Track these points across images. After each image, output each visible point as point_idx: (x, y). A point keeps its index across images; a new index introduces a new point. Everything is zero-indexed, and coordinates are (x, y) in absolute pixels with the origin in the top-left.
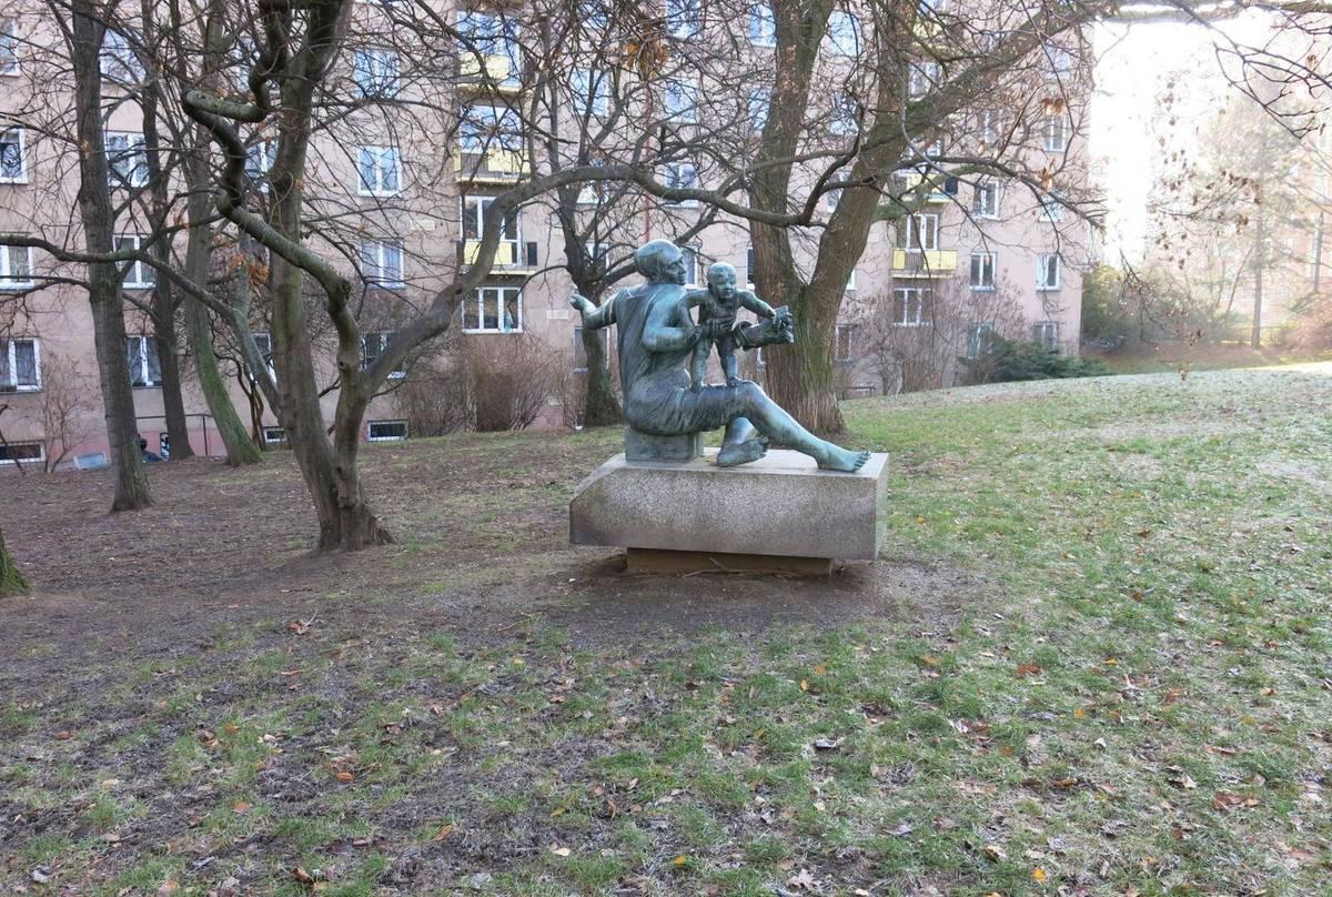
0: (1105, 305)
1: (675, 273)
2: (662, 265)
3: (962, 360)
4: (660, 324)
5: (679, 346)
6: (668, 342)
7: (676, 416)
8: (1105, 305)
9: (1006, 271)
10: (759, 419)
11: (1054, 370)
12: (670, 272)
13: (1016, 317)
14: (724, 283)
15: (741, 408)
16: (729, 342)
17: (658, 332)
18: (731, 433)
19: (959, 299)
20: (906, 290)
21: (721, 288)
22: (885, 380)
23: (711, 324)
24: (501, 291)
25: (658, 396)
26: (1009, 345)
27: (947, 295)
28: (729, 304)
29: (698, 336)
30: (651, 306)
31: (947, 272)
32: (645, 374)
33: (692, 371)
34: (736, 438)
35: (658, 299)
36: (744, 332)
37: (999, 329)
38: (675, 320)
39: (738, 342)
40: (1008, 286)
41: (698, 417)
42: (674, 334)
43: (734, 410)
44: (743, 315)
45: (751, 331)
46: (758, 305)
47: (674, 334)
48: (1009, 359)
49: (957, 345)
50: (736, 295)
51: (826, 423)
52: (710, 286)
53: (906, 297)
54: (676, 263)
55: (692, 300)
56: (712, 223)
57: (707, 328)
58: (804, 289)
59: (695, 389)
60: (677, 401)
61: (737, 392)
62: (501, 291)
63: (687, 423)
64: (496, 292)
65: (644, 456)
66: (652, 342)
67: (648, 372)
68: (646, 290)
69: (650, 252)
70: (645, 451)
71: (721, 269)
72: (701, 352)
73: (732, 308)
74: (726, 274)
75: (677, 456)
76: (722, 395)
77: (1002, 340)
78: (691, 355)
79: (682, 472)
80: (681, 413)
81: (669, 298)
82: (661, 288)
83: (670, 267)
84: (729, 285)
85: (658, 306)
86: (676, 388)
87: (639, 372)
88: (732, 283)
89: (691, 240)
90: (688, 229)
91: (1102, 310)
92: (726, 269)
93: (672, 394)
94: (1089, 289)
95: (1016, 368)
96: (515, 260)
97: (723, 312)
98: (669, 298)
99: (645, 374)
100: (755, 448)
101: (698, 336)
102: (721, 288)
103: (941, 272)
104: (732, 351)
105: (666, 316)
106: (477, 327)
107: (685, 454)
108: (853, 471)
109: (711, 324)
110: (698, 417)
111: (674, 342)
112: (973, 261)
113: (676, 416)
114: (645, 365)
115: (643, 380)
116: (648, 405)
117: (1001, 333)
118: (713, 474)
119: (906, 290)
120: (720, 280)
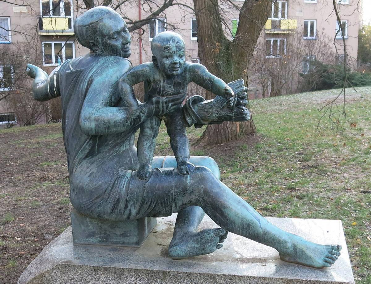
0: (368, 45)
1: (118, 43)
2: (103, 35)
3: (301, 75)
4: (99, 105)
5: (121, 129)
6: (108, 125)
7: (122, 205)
8: (368, 45)
9: (324, 29)
10: (216, 210)
11: (351, 81)
12: (112, 42)
13: (329, 52)
14: (171, 56)
15: (194, 197)
16: (179, 120)
17: (97, 112)
18: (183, 219)
19: (298, 44)
20: (272, 40)
21: (167, 62)
22: (264, 87)
23: (158, 102)
24: (53, 44)
25: (103, 182)
26: (325, 67)
27: (294, 42)
28: (177, 80)
29: (143, 117)
30: (91, 82)
31: (293, 30)
32: (87, 157)
33: (139, 145)
34: (190, 224)
35: (99, 74)
36: (195, 109)
37: (320, 59)
38: (116, 100)
39: (189, 120)
40: (324, 37)
41: (146, 206)
42: (116, 115)
43: (186, 200)
44: (192, 91)
45: (203, 108)
46: (211, 80)
47: (116, 115)
48: (325, 74)
49: (298, 68)
50: (186, 69)
51: (244, 130)
52: (154, 59)
53: (272, 43)
54: (118, 33)
55: (135, 77)
56: (172, 4)
57: (153, 107)
58: (228, 45)
59: (141, 174)
60: (123, 188)
61: (189, 180)
62: (53, 44)
63: (134, 211)
64: (51, 44)
65: (92, 239)
66: (89, 125)
67: (90, 154)
68: (88, 63)
69: (90, 21)
70: (92, 235)
71: (167, 40)
72: (148, 131)
73: (180, 85)
74: (172, 46)
75: (126, 240)
76: (172, 182)
77: (321, 64)
78: (137, 134)
79: (130, 270)
80: (127, 202)
81: (110, 73)
82: (102, 60)
83: (111, 37)
84: (176, 59)
85: (98, 81)
86: (121, 171)
87: (81, 156)
88: (180, 56)
89: (160, 15)
90: (158, 8)
91: (366, 48)
92: (173, 39)
93: (117, 178)
94: (360, 37)
95: (329, 78)
96: (70, 27)
97: (170, 89)
98: (110, 73)
99: (87, 157)
100: (211, 240)
101: (143, 117)
102: (167, 62)
103: (289, 30)
104: (183, 130)
105: (106, 95)
106: (52, 63)
107: (135, 239)
108: (322, 269)
109: (158, 102)
110: (146, 206)
111: (116, 124)
112: (305, 24)
113: (122, 205)
114: (87, 148)
115: (85, 164)
116: (91, 192)
117: (321, 61)
118: (164, 273)
119: (272, 40)
120: (166, 53)
